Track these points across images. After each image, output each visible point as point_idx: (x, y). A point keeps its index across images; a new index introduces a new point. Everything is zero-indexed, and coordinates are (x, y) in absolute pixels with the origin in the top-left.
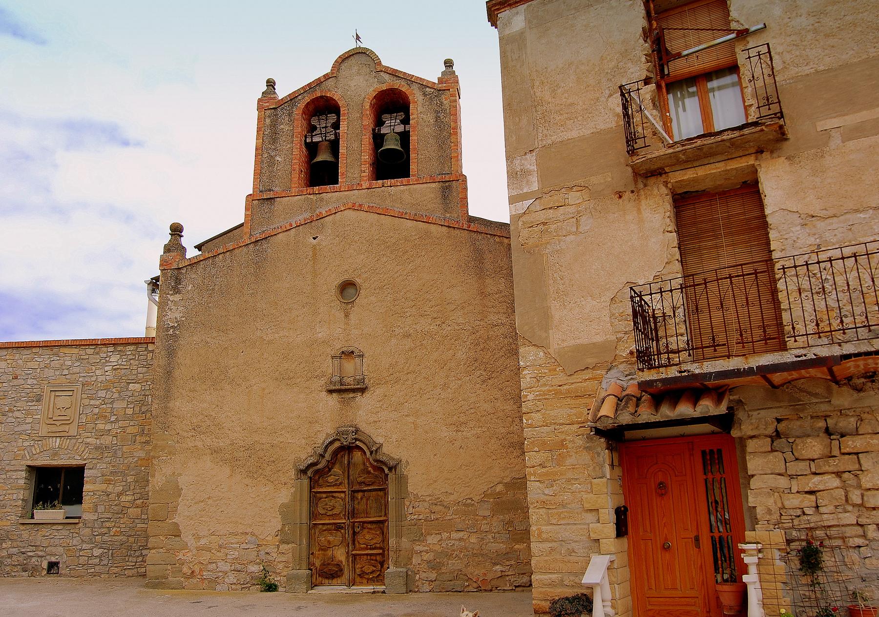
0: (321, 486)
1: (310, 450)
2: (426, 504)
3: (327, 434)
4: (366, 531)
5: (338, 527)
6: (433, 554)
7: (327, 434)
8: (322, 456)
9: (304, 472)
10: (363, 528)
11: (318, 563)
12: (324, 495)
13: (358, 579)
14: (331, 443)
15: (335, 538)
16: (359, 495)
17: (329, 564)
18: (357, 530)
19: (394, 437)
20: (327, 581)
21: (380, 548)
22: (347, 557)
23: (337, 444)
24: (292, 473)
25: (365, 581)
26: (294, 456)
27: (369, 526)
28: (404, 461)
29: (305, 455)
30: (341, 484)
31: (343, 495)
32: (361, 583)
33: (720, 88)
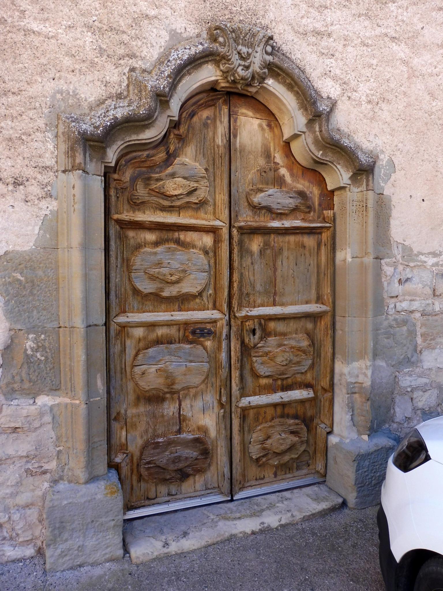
0: (137, 205)
1: (115, 76)
2: (426, 276)
3: (174, 35)
4: (272, 340)
5: (196, 333)
6: (436, 392)
7: (174, 35)
8: (162, 99)
9: (93, 143)
10: (266, 334)
11: (135, 441)
12: (151, 237)
13: (253, 471)
14: (194, 62)
15: (185, 365)
16: (255, 244)
17: (169, 443)
18: (252, 340)
19: (364, 89)
20: (163, 489)
21: (307, 386)
22: (226, 419)
23: (208, 74)
24: (48, 149)
25: (269, 473)
26: (50, 87)
27: (280, 327)
28: (383, 160)
29: (96, 89)
30: (202, 204)
31: (208, 240)
32: (260, 480)
33: (86, 190)
